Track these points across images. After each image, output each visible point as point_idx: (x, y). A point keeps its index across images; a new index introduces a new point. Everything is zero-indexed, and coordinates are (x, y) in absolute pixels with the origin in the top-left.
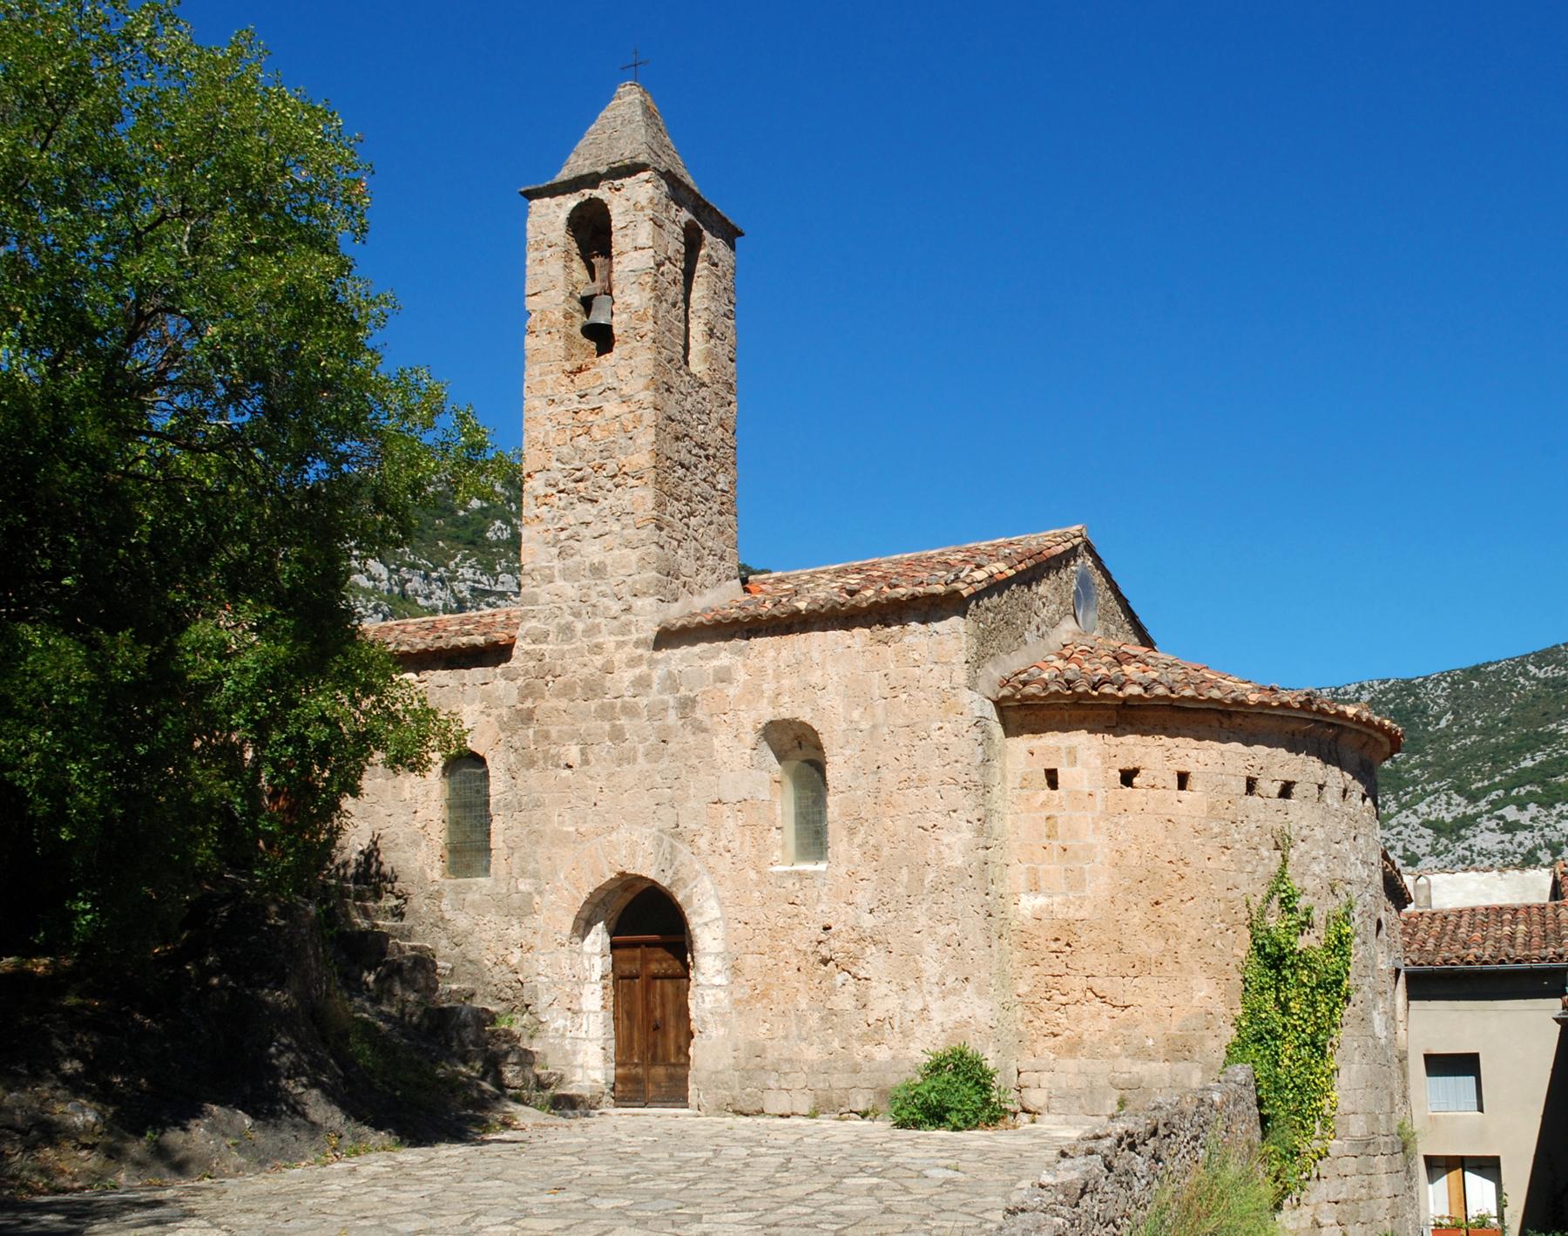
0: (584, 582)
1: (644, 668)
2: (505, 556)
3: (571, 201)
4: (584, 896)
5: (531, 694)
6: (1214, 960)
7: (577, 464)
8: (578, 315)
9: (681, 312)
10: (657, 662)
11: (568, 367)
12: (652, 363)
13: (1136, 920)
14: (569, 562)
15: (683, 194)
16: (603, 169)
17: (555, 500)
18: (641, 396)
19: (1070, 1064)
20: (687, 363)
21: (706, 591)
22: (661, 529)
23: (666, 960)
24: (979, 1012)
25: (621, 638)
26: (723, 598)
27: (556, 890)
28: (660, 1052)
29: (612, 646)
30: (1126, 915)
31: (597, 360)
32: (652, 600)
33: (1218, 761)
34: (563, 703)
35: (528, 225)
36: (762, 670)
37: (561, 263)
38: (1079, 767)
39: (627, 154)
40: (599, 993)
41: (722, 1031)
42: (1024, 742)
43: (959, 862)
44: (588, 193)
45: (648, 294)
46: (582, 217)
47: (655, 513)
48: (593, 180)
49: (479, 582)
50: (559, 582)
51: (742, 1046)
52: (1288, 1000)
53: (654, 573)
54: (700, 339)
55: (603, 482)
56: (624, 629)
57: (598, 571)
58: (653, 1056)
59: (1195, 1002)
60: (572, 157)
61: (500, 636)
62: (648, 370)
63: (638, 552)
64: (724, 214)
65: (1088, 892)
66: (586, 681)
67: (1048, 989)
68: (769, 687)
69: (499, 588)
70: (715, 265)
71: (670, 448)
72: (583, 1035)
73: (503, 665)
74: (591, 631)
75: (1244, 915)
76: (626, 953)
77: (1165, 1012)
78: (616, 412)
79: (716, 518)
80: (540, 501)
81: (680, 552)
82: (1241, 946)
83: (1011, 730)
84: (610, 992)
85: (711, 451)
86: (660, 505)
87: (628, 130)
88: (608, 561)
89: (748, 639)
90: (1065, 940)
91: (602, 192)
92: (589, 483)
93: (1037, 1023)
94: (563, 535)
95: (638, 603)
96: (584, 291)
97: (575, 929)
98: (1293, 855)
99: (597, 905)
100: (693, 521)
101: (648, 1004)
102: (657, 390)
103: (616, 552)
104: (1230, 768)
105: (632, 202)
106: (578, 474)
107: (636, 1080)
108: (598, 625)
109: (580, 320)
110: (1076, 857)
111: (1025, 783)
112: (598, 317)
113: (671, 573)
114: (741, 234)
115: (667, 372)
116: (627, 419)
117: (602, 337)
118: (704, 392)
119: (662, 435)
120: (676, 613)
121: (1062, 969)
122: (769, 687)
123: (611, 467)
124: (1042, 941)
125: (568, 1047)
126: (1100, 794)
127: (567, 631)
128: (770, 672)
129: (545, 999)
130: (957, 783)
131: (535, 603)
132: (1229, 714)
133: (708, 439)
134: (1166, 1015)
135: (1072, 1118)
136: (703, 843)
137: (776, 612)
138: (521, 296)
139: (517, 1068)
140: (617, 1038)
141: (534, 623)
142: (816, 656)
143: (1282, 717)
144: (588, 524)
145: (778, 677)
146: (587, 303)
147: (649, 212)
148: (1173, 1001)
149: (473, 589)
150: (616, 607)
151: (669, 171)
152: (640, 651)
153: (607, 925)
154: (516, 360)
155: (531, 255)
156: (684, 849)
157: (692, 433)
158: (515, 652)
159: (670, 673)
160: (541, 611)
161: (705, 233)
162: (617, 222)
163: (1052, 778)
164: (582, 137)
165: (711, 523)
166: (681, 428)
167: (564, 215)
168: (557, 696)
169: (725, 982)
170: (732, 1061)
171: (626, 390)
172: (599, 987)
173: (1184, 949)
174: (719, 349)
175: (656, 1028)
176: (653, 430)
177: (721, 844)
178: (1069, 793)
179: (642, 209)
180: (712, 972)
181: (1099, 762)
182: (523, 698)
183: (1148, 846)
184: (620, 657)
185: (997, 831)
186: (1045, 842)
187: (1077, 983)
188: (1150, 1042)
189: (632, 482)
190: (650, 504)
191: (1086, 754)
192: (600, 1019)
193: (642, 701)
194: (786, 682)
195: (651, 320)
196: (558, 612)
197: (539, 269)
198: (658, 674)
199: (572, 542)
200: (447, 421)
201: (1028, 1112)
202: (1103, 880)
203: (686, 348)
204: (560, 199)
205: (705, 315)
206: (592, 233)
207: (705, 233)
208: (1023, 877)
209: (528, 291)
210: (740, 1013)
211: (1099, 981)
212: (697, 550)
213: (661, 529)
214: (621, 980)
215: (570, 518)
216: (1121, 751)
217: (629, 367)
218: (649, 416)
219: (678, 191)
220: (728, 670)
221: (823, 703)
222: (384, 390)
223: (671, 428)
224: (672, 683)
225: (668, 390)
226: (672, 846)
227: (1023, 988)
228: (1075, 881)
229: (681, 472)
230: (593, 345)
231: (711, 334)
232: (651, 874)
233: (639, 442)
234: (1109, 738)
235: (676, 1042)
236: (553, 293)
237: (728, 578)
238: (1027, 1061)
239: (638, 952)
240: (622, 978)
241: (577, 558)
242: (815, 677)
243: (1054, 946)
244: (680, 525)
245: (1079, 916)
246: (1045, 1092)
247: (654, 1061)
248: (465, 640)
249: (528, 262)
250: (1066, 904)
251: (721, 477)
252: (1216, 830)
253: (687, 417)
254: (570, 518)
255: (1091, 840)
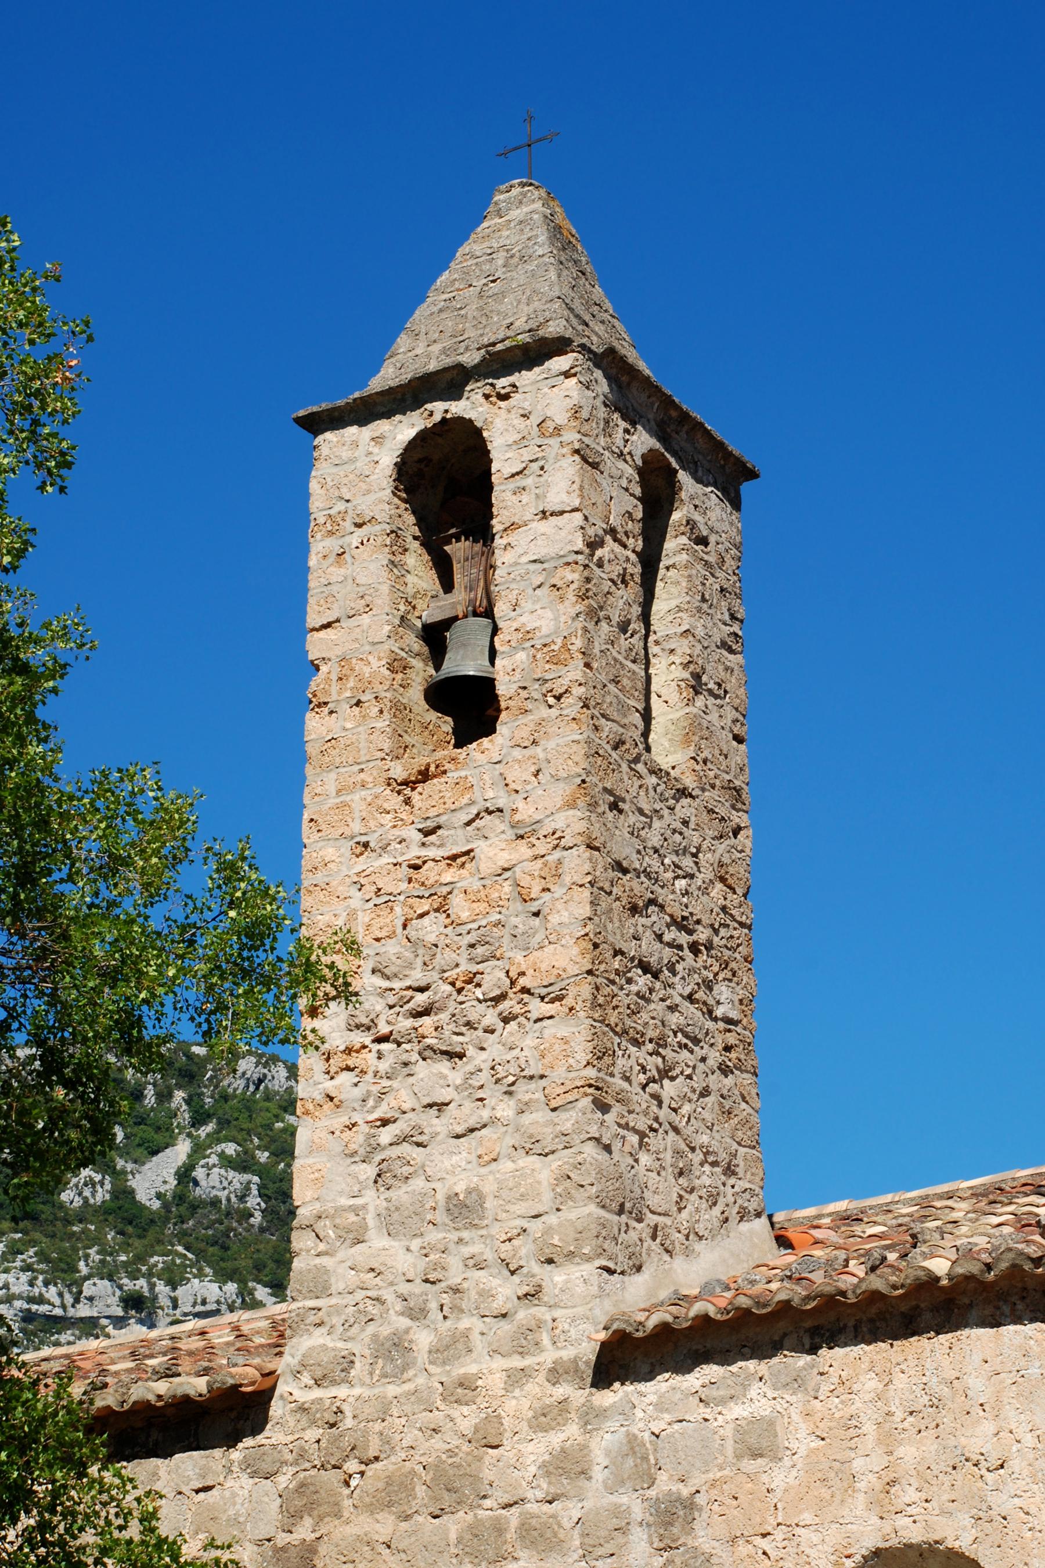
0: (434, 1236)
1: (573, 1430)
2: (97, 1240)
3: (404, 429)
5: (309, 1508)
7: (417, 977)
8: (417, 663)
9: (637, 641)
10: (602, 1414)
11: (399, 771)
12: (581, 750)
14: (401, 1194)
15: (638, 397)
16: (471, 358)
17: (368, 1059)
18: (559, 821)
20: (648, 749)
21: (699, 1247)
22: (604, 1108)
25: (517, 1362)
26: (722, 1263)
29: (495, 1382)
31: (462, 752)
32: (589, 1269)
34: (384, 1526)
35: (314, 486)
36: (851, 1424)
37: (384, 557)
39: (520, 324)
44: (439, 408)
45: (571, 606)
46: (426, 460)
47: (591, 1073)
48: (450, 382)
49: (41, 1300)
50: (377, 1241)
53: (592, 1208)
54: (674, 697)
55: (475, 1012)
56: (525, 1341)
57: (464, 1209)
60: (403, 342)
61: (244, 1373)
62: (575, 763)
63: (554, 1163)
64: (719, 436)
66: (437, 1468)
68: (867, 1465)
69: (84, 1311)
70: (703, 541)
71: (620, 930)
73: (248, 1442)
74: (448, 1349)
78: (504, 858)
79: (716, 1081)
80: (336, 1062)
81: (645, 1159)
85: (702, 935)
86: (601, 1055)
87: (520, 276)
88: (489, 1187)
89: (813, 1350)
91: (470, 406)
92: (444, 1017)
94: (386, 1135)
95: (556, 1278)
96: (430, 613)
100: (669, 1089)
102: (593, 806)
103: (506, 1166)
105: (535, 420)
106: (421, 999)
108: (466, 1335)
109: (421, 672)
112: (464, 661)
113: (627, 1207)
114: (752, 475)
115: (612, 768)
116: (529, 874)
117: (470, 707)
118: (685, 808)
119: (605, 901)
120: (642, 1299)
122: (867, 1465)
123: (494, 979)
127: (394, 1351)
128: (869, 1428)
131: (324, 1291)
133: (697, 909)
137: (876, 1283)
138: (298, 630)
141: (318, 1338)
142: (977, 1384)
144: (440, 1106)
145: (888, 1440)
146: (435, 638)
147: (571, 436)
149: (28, 1317)
150: (505, 1290)
151: (611, 351)
152: (561, 1391)
154: (289, 765)
155: (320, 546)
157: (663, 895)
158: (277, 1409)
159: (632, 1440)
160: (336, 1309)
161: (683, 476)
162: (503, 462)
164: (423, 298)
165: (705, 1093)
166: (640, 887)
167: (388, 458)
168: (372, 1509)
171: (526, 812)
174: (714, 717)
176: (586, 894)
179: (558, 430)
182: (292, 1517)
184: (517, 1406)
189: (538, 1008)
190: (582, 1053)
193: (569, 1511)
194: (908, 1453)
195: (579, 662)
196: (374, 1310)
197: (336, 573)
198: (603, 1445)
199: (406, 1149)
200: (197, 878)
203: (647, 716)
204: (381, 426)
205: (683, 647)
206: (449, 493)
207: (683, 476)
209: (313, 619)
212: (678, 1153)
213: (604, 1108)
215: (403, 1096)
217: (534, 761)
218: (577, 864)
219: (630, 392)
220: (768, 1425)
221: (1003, 1503)
222: (65, 817)
223: (624, 887)
224: (639, 1462)
225: (614, 806)
229: (642, 981)
230: (447, 725)
231: (697, 684)
233: (554, 919)
236: (366, 619)
237: (743, 1215)
241: (418, 1183)
242: (979, 1438)
244: (642, 1099)
248: (162, 1387)
249: (313, 562)
251: (723, 991)
253: (655, 864)
254: (403, 1096)
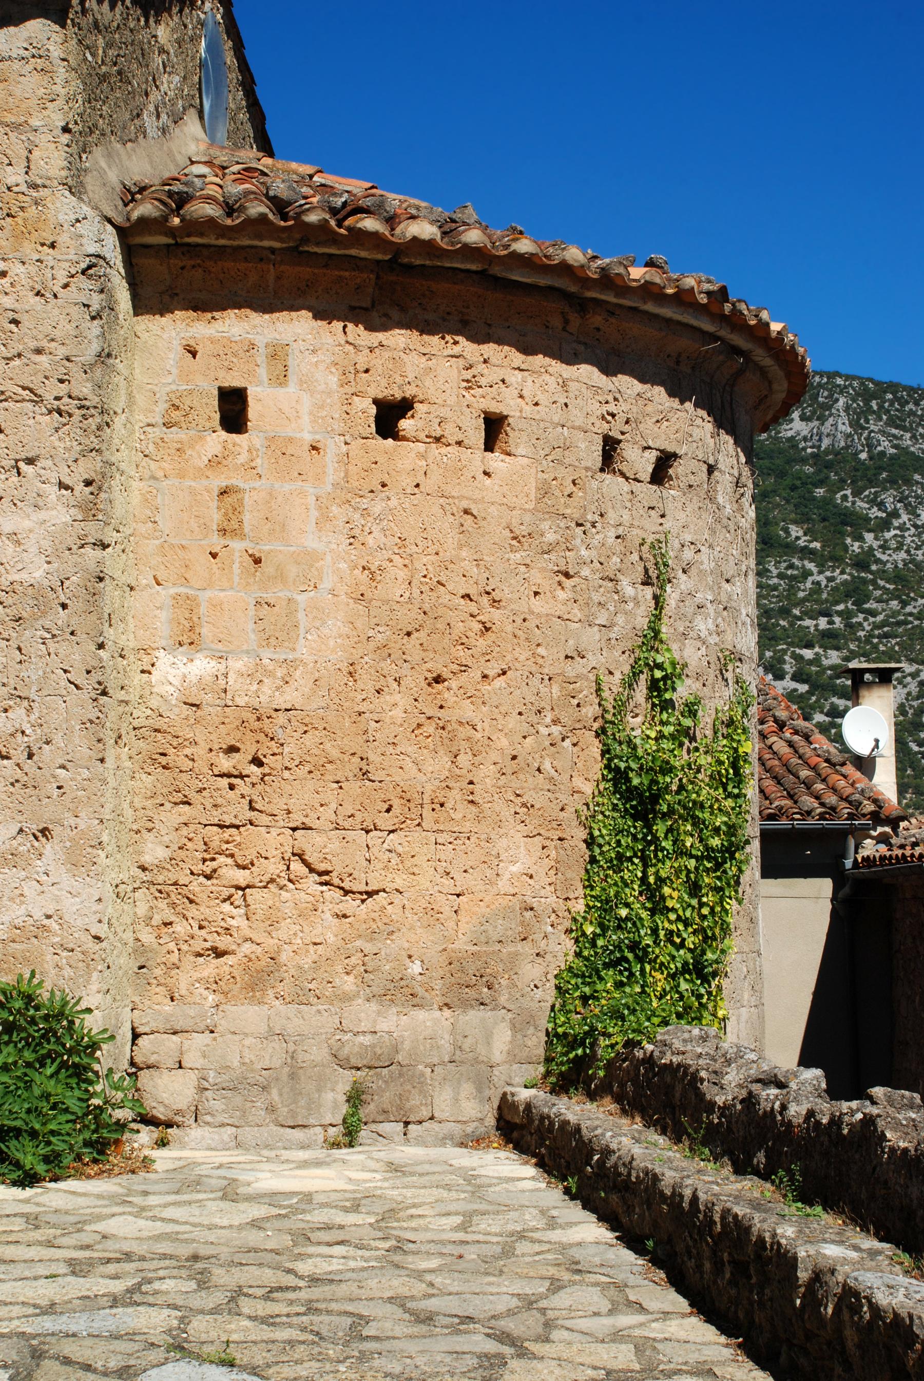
6: (538, 799)
13: (398, 713)
19: (249, 1016)
24: (70, 905)
30: (377, 702)
33: (558, 397)
38: (292, 388)
42: (172, 330)
43: (37, 572)
52: (661, 881)
59: (503, 885)
65: (303, 651)
67: (210, 854)
75: (591, 710)
77: (445, 905)
82: (583, 773)
83: (150, 299)
90: (251, 751)
93: (180, 928)
98: (672, 595)
104: (577, 416)
110: (281, 576)
111: (176, 413)
121: (237, 811)
124: (200, 751)
126: (333, 447)
130: (38, 400)
132: (583, 306)
134: (447, 911)
135: (248, 1134)
143: (668, 321)
148: (462, 882)
163: (233, 410)
173: (486, 775)
178: (272, 439)
181: (333, 380)
183: (424, 562)
185: (118, 511)
186: (216, 542)
187: (270, 842)
188: (416, 968)
191: (306, 365)
201: (147, 1120)
202: (335, 626)
208: (164, 615)
211: (316, 839)
216: (378, 361)
227: (154, 851)
228: (275, 626)
234: (357, 332)
238: (157, 1010)
243: (225, 763)
245: (282, 701)
246: (193, 1076)
250: (256, 675)
252: (550, 537)
255: (312, 542)
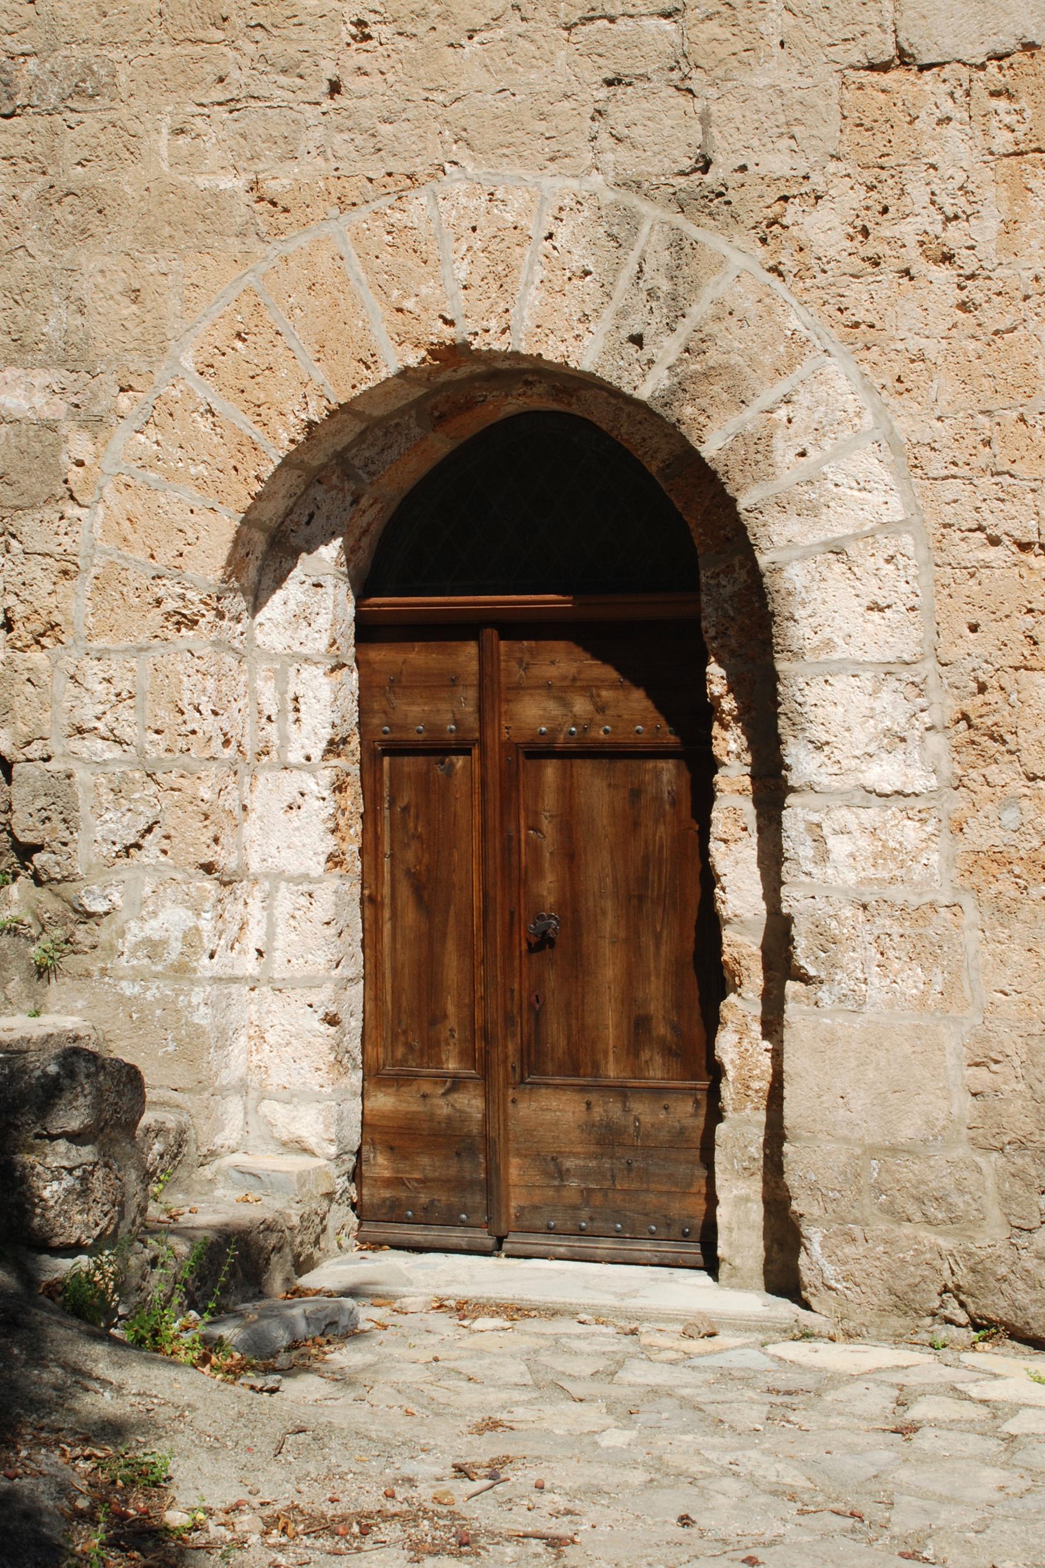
4: (281, 439)
23: (576, 684)
27: (161, 414)
28: (555, 1033)
40: (319, 808)
41: (911, 981)
51: (1010, 1042)
58: (522, 1048)
72: (250, 966)
76: (417, 657)
84: (353, 800)
97: (235, 565)
99: (316, 478)
101: (510, 846)
107: (446, 1138)
125: (202, 1017)
129: (104, 826)
136: (823, 228)
139: (87, 1153)
140: (372, 976)
153: (350, 551)
156: (733, 261)
169: (920, 781)
170: (964, 1106)
172: (317, 784)
175: (542, 943)
177: (908, 230)
180: (861, 737)
192: (324, 906)
210: (1004, 911)
214: (394, 765)
226: (678, 244)
232: (587, 354)
235: (629, 998)
239: (467, 655)
240: (396, 750)
247: (533, 1067)
